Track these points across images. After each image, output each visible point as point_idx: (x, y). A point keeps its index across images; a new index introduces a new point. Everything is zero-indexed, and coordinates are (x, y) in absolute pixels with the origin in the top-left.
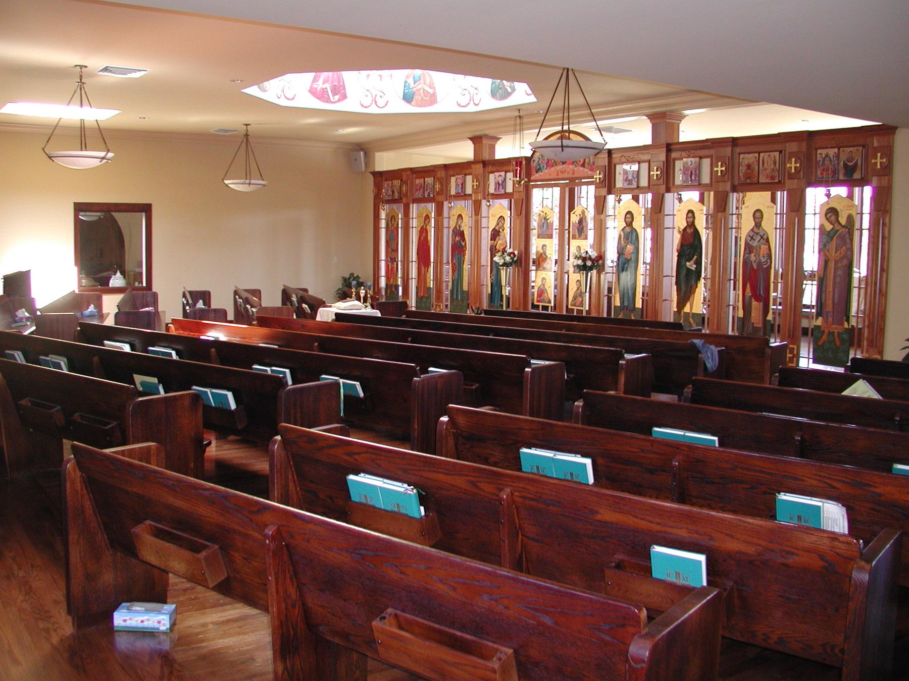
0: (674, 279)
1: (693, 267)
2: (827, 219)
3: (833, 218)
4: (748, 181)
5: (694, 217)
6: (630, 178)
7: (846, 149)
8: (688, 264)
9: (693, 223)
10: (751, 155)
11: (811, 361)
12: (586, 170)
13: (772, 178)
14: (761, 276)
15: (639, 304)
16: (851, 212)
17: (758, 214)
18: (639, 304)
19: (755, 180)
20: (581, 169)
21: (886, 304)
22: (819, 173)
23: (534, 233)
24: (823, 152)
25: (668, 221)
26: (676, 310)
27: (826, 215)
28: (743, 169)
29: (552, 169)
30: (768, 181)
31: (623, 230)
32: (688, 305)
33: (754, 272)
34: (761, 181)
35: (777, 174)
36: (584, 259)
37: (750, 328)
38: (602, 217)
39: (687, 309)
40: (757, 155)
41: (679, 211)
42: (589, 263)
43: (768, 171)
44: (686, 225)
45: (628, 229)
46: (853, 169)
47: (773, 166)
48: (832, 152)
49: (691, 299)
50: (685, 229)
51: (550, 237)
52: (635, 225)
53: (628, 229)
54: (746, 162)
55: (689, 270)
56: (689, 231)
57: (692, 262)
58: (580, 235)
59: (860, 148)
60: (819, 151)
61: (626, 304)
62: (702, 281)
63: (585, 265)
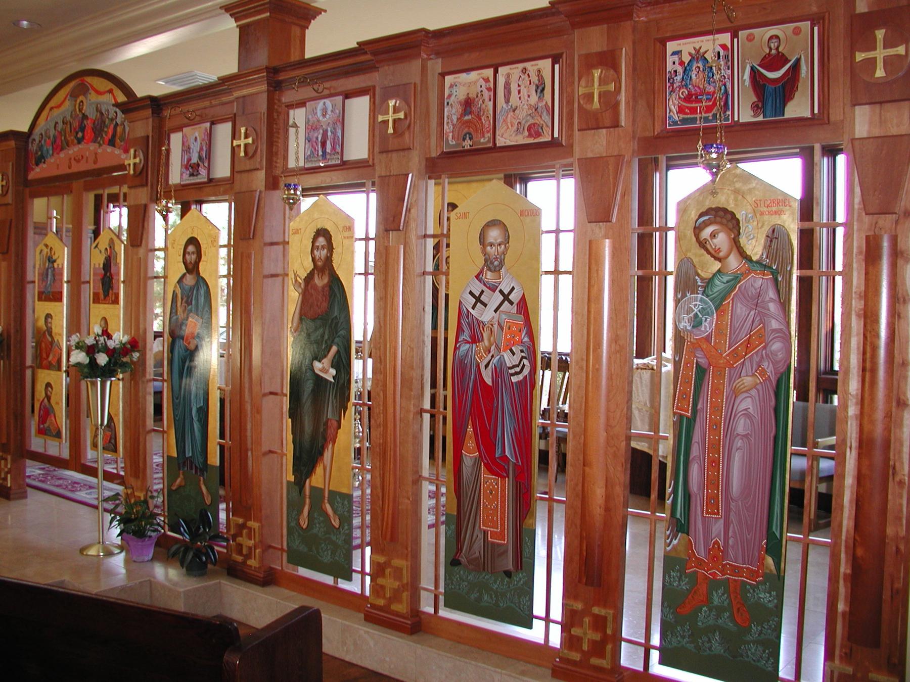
0: (286, 401)
1: (330, 374)
2: (702, 244)
3: (722, 241)
4: (467, 144)
5: (330, 247)
6: (195, 160)
7: (756, 31)
8: (317, 365)
9: (329, 260)
10: (474, 75)
11: (655, 655)
12: (117, 152)
13: (533, 130)
14: (506, 403)
15: (214, 459)
16: (776, 220)
17: (494, 235)
18: (214, 459)
19: (484, 141)
20: (109, 149)
21: (142, 234)
22: (673, 104)
23: (31, 292)
24: (687, 47)
25: (270, 261)
26: (292, 478)
27: (697, 230)
28: (452, 112)
29: (62, 155)
30: (523, 139)
31: (180, 281)
32: (319, 470)
33: (488, 393)
34: (500, 142)
35: (547, 118)
36: (91, 350)
37: (479, 544)
38: (141, 251)
39: (317, 479)
40: (489, 72)
41: (297, 232)
42: (102, 359)
43: (522, 114)
44: (310, 266)
45: (190, 280)
46: (788, 88)
47: (534, 99)
48: (709, 45)
49: (327, 455)
50: (309, 279)
51: (58, 298)
52: (204, 269)
53: (190, 280)
54: (460, 94)
55: (319, 381)
56: (320, 282)
57: (326, 362)
58: (106, 295)
59: (806, 25)
60: (671, 46)
61: (189, 454)
62: (351, 410)
63: (93, 363)
